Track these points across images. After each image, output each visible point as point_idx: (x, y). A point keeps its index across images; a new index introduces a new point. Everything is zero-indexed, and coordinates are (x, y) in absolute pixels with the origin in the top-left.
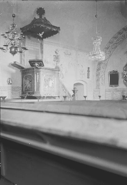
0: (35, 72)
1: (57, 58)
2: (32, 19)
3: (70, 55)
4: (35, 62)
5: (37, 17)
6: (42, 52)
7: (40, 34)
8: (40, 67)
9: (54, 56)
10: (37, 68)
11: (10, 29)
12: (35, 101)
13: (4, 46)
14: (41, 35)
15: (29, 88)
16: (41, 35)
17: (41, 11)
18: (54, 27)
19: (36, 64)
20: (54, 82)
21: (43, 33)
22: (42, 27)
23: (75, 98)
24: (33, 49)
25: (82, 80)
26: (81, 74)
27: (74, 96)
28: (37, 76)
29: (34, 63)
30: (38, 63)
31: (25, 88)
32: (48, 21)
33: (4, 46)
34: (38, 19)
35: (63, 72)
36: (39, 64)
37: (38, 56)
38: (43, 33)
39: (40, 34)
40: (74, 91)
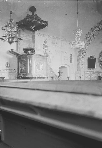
0: (28, 58)
1: (46, 46)
2: (26, 15)
3: (56, 44)
4: (28, 50)
5: (30, 14)
6: (34, 42)
7: (32, 27)
8: (32, 54)
9: (43, 44)
10: (30, 54)
11: (8, 23)
12: (28, 81)
13: (3, 36)
14: (33, 28)
15: (23, 70)
16: (33, 28)
17: (33, 9)
18: (43, 21)
19: (29, 51)
20: (43, 65)
21: (34, 26)
22: (34, 21)
23: (60, 79)
24: (26, 39)
25: (66, 64)
26: (65, 59)
27: (60, 77)
28: (29, 61)
29: (28, 51)
30: (30, 51)
31: (20, 70)
32: (39, 17)
33: (3, 36)
34: (31, 15)
35: (50, 58)
36: (31, 51)
37: (30, 45)
38: (34, 26)
39: (32, 27)
40: (59, 73)
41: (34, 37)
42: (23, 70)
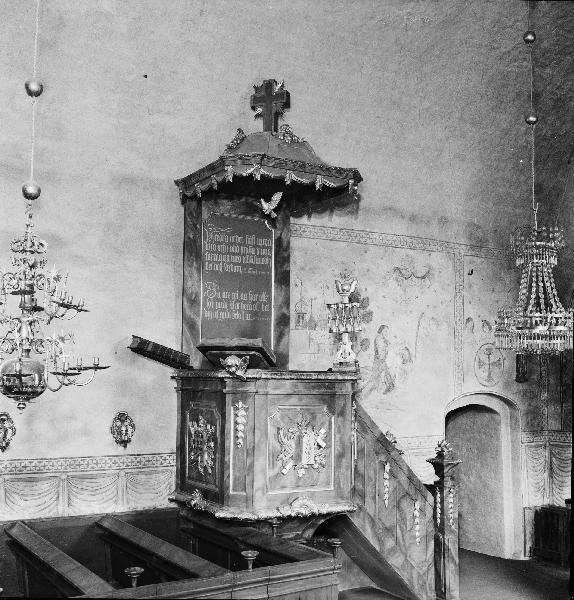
0: (229, 398)
1: (352, 308)
3: (423, 277)
6: (284, 279)
7: (263, 203)
8: (251, 373)
9: (329, 306)
10: (239, 378)
13: (43, 309)
14: (267, 207)
16: (267, 207)
17: (271, 100)
20: (327, 439)
21: (277, 197)
23: (442, 502)
24: (237, 269)
25: (487, 390)
27: (442, 491)
29: (225, 357)
30: (240, 356)
31: (191, 463)
32: (304, 144)
33: (43, 309)
35: (388, 361)
36: (245, 361)
38: (277, 197)
39: (263, 203)
40: (438, 466)
41: (287, 260)
42: (205, 468)
